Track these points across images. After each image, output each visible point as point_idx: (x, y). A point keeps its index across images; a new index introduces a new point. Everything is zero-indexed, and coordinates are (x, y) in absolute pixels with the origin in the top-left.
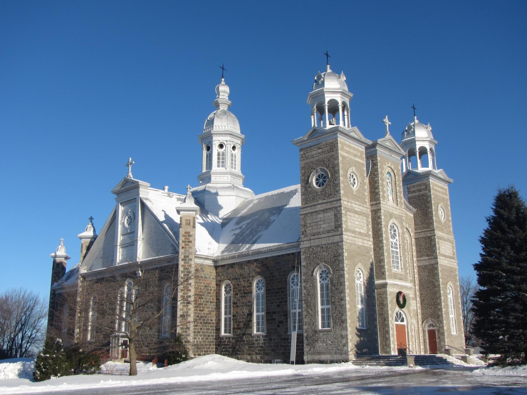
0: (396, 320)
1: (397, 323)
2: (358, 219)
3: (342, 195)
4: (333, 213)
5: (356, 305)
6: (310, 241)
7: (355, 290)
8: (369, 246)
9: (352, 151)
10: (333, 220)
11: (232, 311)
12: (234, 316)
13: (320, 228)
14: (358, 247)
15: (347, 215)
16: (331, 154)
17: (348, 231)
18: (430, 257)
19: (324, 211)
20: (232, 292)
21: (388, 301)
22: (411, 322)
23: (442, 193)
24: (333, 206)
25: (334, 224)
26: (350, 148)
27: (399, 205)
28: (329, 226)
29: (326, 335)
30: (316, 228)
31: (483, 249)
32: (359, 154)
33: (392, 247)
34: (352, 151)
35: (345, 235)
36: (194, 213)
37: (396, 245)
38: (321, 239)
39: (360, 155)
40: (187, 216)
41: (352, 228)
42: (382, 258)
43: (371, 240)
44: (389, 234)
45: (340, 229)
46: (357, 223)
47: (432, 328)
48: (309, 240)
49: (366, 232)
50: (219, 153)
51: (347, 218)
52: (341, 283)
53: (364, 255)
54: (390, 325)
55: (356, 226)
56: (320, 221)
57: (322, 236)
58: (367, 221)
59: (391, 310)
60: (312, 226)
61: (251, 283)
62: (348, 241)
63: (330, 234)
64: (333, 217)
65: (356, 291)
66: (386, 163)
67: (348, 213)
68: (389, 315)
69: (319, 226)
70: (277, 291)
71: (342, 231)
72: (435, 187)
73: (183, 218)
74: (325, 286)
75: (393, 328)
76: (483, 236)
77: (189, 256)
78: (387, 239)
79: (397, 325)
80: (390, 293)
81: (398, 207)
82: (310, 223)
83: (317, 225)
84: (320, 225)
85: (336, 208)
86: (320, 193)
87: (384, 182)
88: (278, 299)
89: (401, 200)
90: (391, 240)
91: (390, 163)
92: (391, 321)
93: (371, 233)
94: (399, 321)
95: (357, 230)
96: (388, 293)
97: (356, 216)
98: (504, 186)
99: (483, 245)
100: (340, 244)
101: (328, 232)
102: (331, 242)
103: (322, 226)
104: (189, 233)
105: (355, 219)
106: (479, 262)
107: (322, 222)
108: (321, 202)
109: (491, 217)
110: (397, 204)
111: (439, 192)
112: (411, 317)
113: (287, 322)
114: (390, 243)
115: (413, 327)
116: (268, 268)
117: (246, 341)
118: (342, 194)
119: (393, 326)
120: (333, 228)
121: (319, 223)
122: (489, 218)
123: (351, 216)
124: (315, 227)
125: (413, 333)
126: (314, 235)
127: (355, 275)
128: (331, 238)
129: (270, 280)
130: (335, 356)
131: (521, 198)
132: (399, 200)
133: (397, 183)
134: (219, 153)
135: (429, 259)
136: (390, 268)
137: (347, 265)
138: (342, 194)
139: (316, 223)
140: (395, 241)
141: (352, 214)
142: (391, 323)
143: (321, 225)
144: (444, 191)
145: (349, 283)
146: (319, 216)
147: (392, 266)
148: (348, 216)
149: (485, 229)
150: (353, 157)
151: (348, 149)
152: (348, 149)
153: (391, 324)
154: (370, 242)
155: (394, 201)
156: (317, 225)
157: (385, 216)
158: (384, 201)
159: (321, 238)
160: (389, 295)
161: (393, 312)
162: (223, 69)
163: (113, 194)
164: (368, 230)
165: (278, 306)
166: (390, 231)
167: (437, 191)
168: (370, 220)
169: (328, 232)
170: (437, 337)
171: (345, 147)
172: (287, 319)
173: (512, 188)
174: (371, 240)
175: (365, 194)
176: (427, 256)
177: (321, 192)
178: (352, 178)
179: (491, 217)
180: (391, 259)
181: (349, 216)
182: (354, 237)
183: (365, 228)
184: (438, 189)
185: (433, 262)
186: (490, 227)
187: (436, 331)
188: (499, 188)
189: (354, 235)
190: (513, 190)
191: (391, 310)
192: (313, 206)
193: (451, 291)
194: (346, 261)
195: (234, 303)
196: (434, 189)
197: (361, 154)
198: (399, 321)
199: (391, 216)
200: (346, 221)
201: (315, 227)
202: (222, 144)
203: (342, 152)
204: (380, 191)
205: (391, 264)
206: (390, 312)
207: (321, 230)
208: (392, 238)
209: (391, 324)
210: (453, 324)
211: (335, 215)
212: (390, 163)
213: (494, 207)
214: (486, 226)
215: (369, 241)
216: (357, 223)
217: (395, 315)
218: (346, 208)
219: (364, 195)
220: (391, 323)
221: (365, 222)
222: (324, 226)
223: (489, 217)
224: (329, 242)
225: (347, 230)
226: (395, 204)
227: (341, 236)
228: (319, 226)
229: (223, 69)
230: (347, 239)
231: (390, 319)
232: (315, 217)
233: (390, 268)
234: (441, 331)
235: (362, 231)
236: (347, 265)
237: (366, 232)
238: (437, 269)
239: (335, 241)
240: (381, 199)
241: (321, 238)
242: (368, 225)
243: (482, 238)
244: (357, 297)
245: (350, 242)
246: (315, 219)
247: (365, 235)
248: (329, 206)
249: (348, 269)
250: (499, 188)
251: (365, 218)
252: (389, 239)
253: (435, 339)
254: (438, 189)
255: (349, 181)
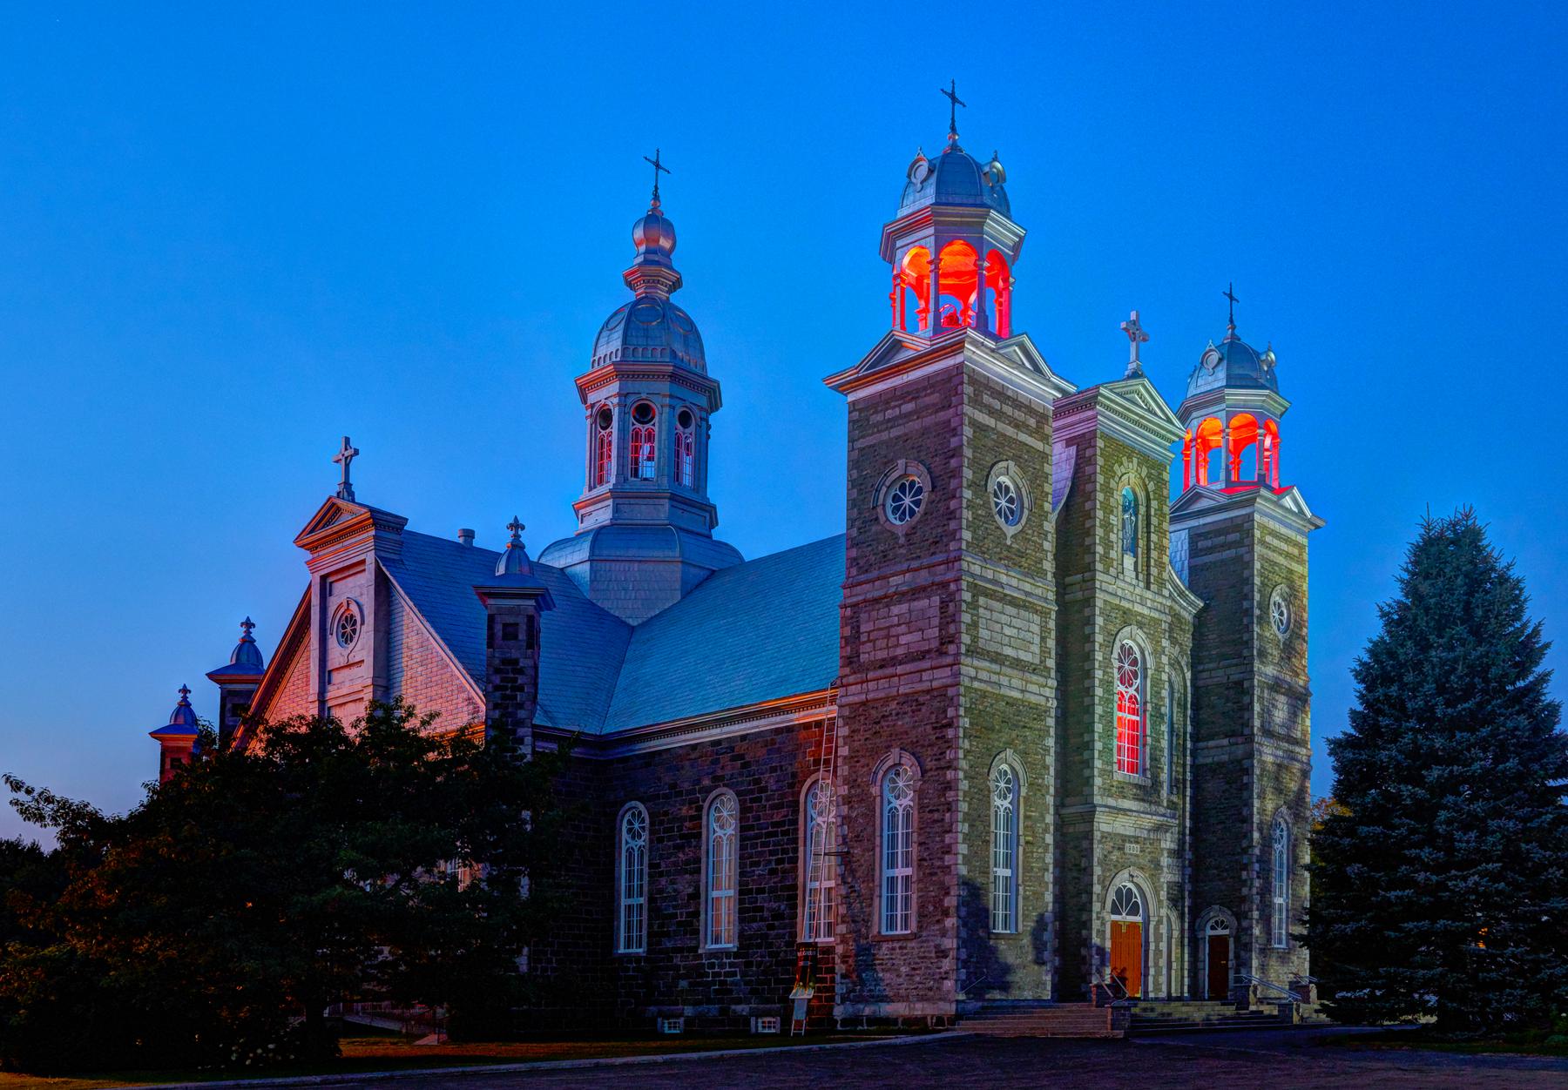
0: (1115, 911)
1: (1115, 917)
2: (1014, 620)
3: (967, 546)
4: (936, 600)
5: (988, 867)
6: (865, 685)
7: (989, 826)
8: (1042, 701)
9: (1008, 410)
10: (936, 621)
11: (645, 889)
12: (651, 900)
13: (898, 645)
14: (1007, 703)
15: (979, 606)
16: (942, 416)
17: (978, 653)
18: (1233, 740)
19: (917, 592)
20: (645, 835)
21: (1096, 859)
22: (1159, 916)
23: (1288, 555)
24: (938, 579)
25: (936, 632)
26: (1001, 402)
27: (1152, 586)
28: (923, 640)
29: (901, 948)
30: (884, 645)
31: (1362, 697)
32: (1032, 422)
33: (1120, 708)
34: (1008, 410)
35: (967, 666)
36: (532, 602)
37: (1133, 703)
38: (897, 678)
39: (1034, 426)
40: (511, 611)
41: (993, 647)
42: (1086, 738)
43: (1049, 685)
44: (1116, 671)
45: (952, 648)
46: (1007, 631)
47: (1220, 932)
48: (862, 683)
49: (1037, 661)
50: (637, 433)
51: (977, 615)
52: (949, 803)
53: (1025, 727)
54: (1096, 924)
55: (1006, 641)
56: (899, 625)
57: (900, 669)
58: (1044, 628)
59: (1102, 881)
60: (874, 641)
61: (700, 809)
62: (976, 685)
63: (926, 664)
64: (935, 611)
65: (992, 828)
66: (1124, 459)
67: (982, 600)
68: (1095, 897)
69: (895, 639)
70: (770, 829)
71: (958, 654)
72: (1268, 539)
73: (498, 619)
74: (900, 813)
75: (1104, 931)
76: (1366, 658)
77: (516, 730)
78: (1107, 686)
79: (1115, 924)
80: (1102, 837)
81: (1149, 595)
82: (869, 632)
83: (888, 637)
84: (898, 636)
85: (944, 585)
86: (902, 540)
87: (1112, 517)
88: (772, 853)
89: (1160, 573)
90: (1122, 688)
91: (1135, 460)
92: (1098, 913)
93: (1051, 663)
94: (1124, 914)
95: (1008, 651)
96: (1097, 835)
97: (1010, 610)
98: (1444, 513)
99: (1361, 687)
100: (950, 692)
101: (923, 655)
102: (926, 686)
103: (903, 640)
104: (516, 662)
105: (1004, 619)
106: (1345, 734)
107: (903, 628)
108: (898, 568)
109: (1394, 604)
110: (1148, 587)
111: (1280, 552)
112: (1160, 901)
113: (795, 916)
114: (1116, 697)
115: (1163, 929)
116: (745, 765)
117: (684, 968)
118: (968, 542)
119: (1103, 924)
120: (935, 644)
121: (893, 631)
122: (1387, 609)
123: (991, 611)
124: (881, 643)
125: (1163, 946)
126: (881, 667)
127: (992, 785)
128: (925, 676)
129: (752, 801)
130: (919, 1006)
131: (1488, 549)
132: (1154, 571)
133: (1154, 521)
134: (637, 433)
135: (1231, 744)
136: (1109, 768)
137: (967, 752)
138: (968, 542)
139: (885, 632)
140: (1132, 691)
141: (997, 605)
142: (1098, 918)
143: (901, 638)
144: (1296, 552)
145: (970, 804)
146: (895, 610)
147: (1115, 760)
148: (981, 611)
149: (1375, 639)
150: (1010, 431)
151: (997, 404)
152: (997, 404)
153: (1099, 922)
154: (1047, 689)
155: (1141, 576)
156: (888, 637)
157: (1107, 618)
158: (1106, 572)
159: (896, 675)
160: (1100, 842)
161: (1106, 889)
162: (658, 166)
163: (303, 550)
164: (1044, 652)
165: (773, 872)
166: (1121, 660)
167: (1274, 551)
168: (1052, 624)
169: (923, 655)
170: (1231, 955)
171: (985, 396)
172: (795, 907)
173: (1467, 516)
174: (1049, 685)
175: (1042, 545)
176: (1226, 736)
177: (907, 535)
178: (1006, 496)
179: (1394, 604)
180: (1115, 742)
181: (985, 608)
182: (995, 673)
183: (1036, 649)
184: (1276, 542)
185: (1240, 751)
186: (1389, 632)
187: (1231, 940)
188: (1426, 517)
189: (995, 667)
190: (1470, 522)
191: (1102, 881)
192: (878, 579)
193: (1285, 833)
194: (966, 741)
195: (651, 866)
196: (1265, 542)
197: (1038, 422)
198: (1124, 914)
199: (1127, 617)
200: (974, 625)
201: (881, 643)
202: (637, 408)
203: (976, 412)
204: (1097, 541)
205: (1112, 755)
206: (1097, 889)
207: (900, 651)
208: (1123, 683)
209: (1099, 922)
210: (1280, 920)
211: (944, 605)
212: (1135, 460)
213: (1406, 576)
214: (1376, 629)
215: (1046, 686)
216: (1007, 631)
217: (1111, 896)
218: (974, 588)
219: (1041, 548)
220: (1098, 918)
221: (1036, 629)
222: (908, 640)
223: (1389, 606)
224: (919, 687)
225: (973, 652)
226: (1141, 584)
227: (955, 667)
228: (892, 641)
229: (658, 166)
230: (973, 679)
231: (1096, 907)
232: (883, 612)
233: (1109, 768)
234: (1245, 939)
235: (1023, 656)
236: (967, 752)
237: (1037, 661)
238: (1248, 771)
239: (935, 684)
240: (1099, 566)
241: (896, 675)
242: (1043, 639)
243: (1363, 664)
244: (992, 845)
245: (983, 686)
246: (884, 618)
247: (1034, 670)
248: (923, 578)
249: (971, 767)
250: (1426, 517)
251: (1037, 618)
252: (1112, 682)
253: (1227, 960)
254: (1276, 542)
255: (993, 505)
